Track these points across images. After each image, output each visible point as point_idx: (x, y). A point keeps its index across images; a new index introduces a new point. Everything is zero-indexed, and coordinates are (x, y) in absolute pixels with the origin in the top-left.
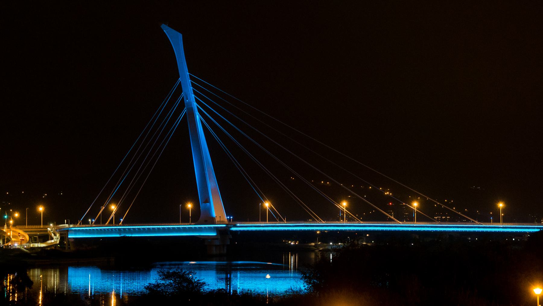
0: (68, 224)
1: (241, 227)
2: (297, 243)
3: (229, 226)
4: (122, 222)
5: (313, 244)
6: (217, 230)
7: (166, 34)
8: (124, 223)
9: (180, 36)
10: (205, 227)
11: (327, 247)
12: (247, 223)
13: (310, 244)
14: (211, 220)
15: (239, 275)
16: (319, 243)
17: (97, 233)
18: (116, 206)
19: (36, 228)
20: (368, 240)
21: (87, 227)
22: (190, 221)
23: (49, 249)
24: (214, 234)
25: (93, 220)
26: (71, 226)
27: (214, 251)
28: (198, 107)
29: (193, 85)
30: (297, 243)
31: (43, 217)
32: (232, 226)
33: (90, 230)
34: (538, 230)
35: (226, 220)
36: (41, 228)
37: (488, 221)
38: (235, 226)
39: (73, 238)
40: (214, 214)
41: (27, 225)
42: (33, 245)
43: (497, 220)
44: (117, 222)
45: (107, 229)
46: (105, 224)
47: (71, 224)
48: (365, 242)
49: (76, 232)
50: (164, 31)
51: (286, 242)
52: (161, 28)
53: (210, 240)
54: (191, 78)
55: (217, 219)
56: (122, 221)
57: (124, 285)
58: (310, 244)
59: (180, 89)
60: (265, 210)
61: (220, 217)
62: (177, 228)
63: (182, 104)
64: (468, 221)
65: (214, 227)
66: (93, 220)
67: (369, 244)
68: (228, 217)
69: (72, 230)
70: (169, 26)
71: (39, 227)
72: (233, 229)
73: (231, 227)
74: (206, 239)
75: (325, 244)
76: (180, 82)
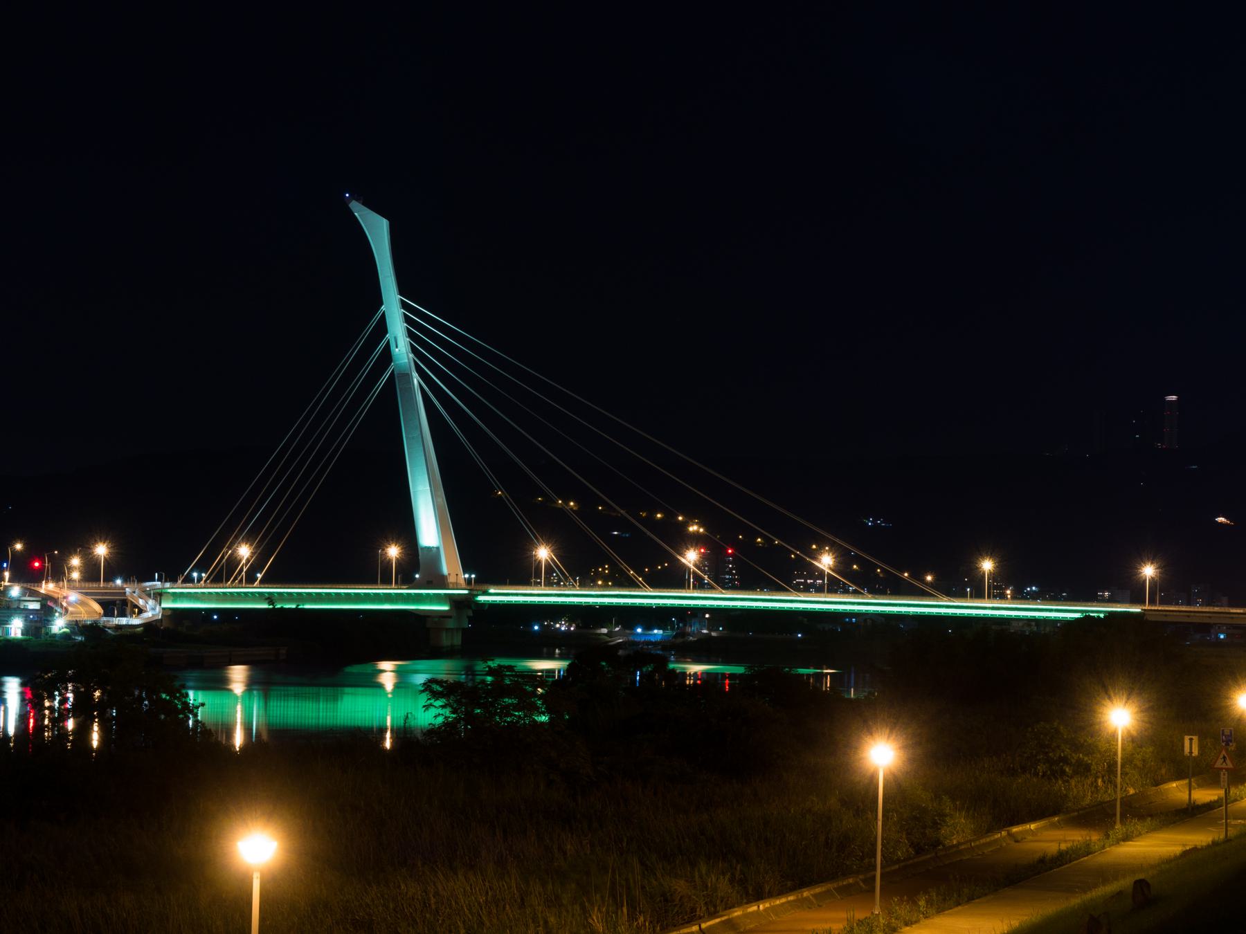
0: (161, 582)
1: (497, 595)
2: (572, 629)
3: (475, 593)
4: (260, 581)
5: (605, 631)
6: (452, 600)
7: (358, 220)
8: (264, 582)
9: (384, 224)
10: (428, 594)
11: (631, 638)
12: (506, 587)
13: (598, 631)
14: (441, 582)
15: (871, 723)
16: (617, 629)
17: (217, 600)
18: (251, 545)
19: (92, 588)
20: (712, 624)
21: (198, 588)
22: (748, 583)
23: (689, 660)
24: (446, 608)
25: (203, 575)
26: (168, 585)
27: (446, 641)
28: (414, 360)
29: (407, 320)
30: (572, 629)
31: (560, 563)
32: (479, 592)
33: (203, 593)
34: (1078, 615)
35: (462, 582)
36: (99, 588)
37: (962, 595)
38: (485, 593)
39: (170, 609)
40: (445, 570)
41: (104, 581)
42: (119, 620)
43: (978, 594)
44: (251, 579)
45: (237, 593)
46: (254, 583)
47: (166, 581)
48: (708, 629)
49: (176, 596)
50: (356, 214)
51: (552, 626)
52: (349, 208)
53: (437, 619)
54: (404, 306)
55: (452, 579)
56: (259, 579)
57: (335, 714)
58: (598, 631)
59: (382, 328)
60: (390, 562)
61: (457, 575)
62: (355, 594)
63: (387, 356)
64: (786, 590)
65: (445, 594)
66: (203, 575)
67: (714, 634)
68: (467, 576)
69: (169, 593)
70: (363, 204)
71: (95, 585)
72: (481, 598)
73: (478, 595)
74: (429, 616)
75: (628, 631)
76: (384, 312)
